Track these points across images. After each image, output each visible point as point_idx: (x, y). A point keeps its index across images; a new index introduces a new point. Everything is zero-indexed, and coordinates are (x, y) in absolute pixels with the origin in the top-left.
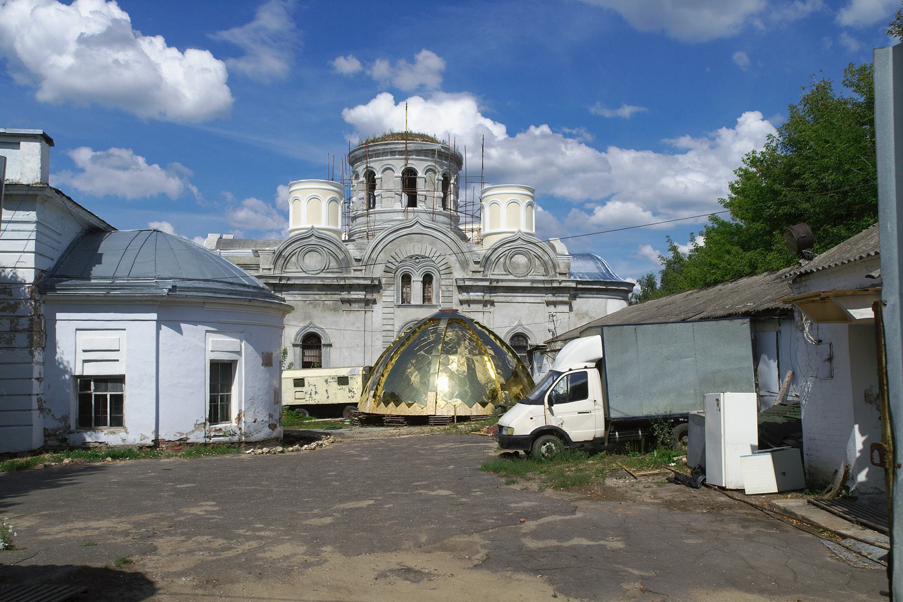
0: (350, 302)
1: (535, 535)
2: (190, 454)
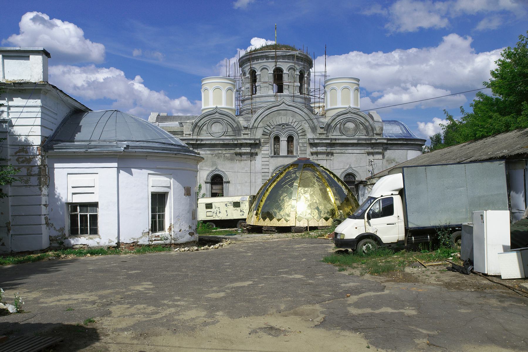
0: (241, 154)
1: (357, 305)
2: (139, 252)
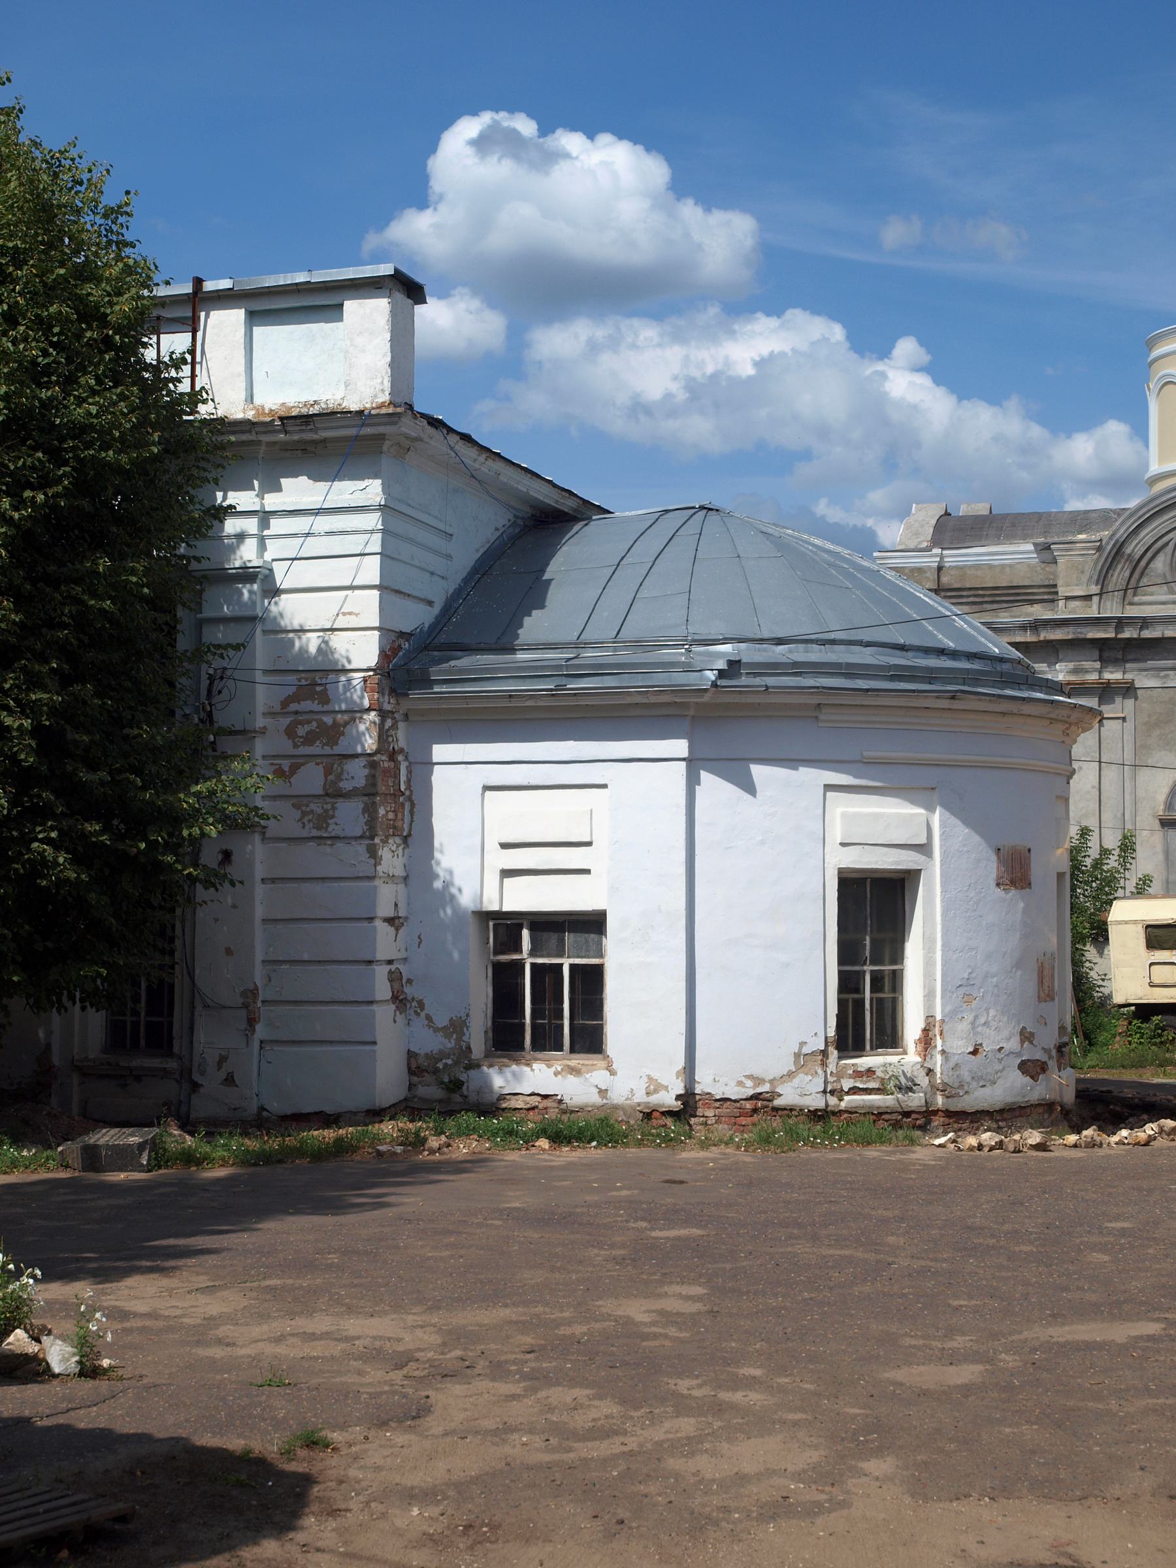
2: (766, 1140)
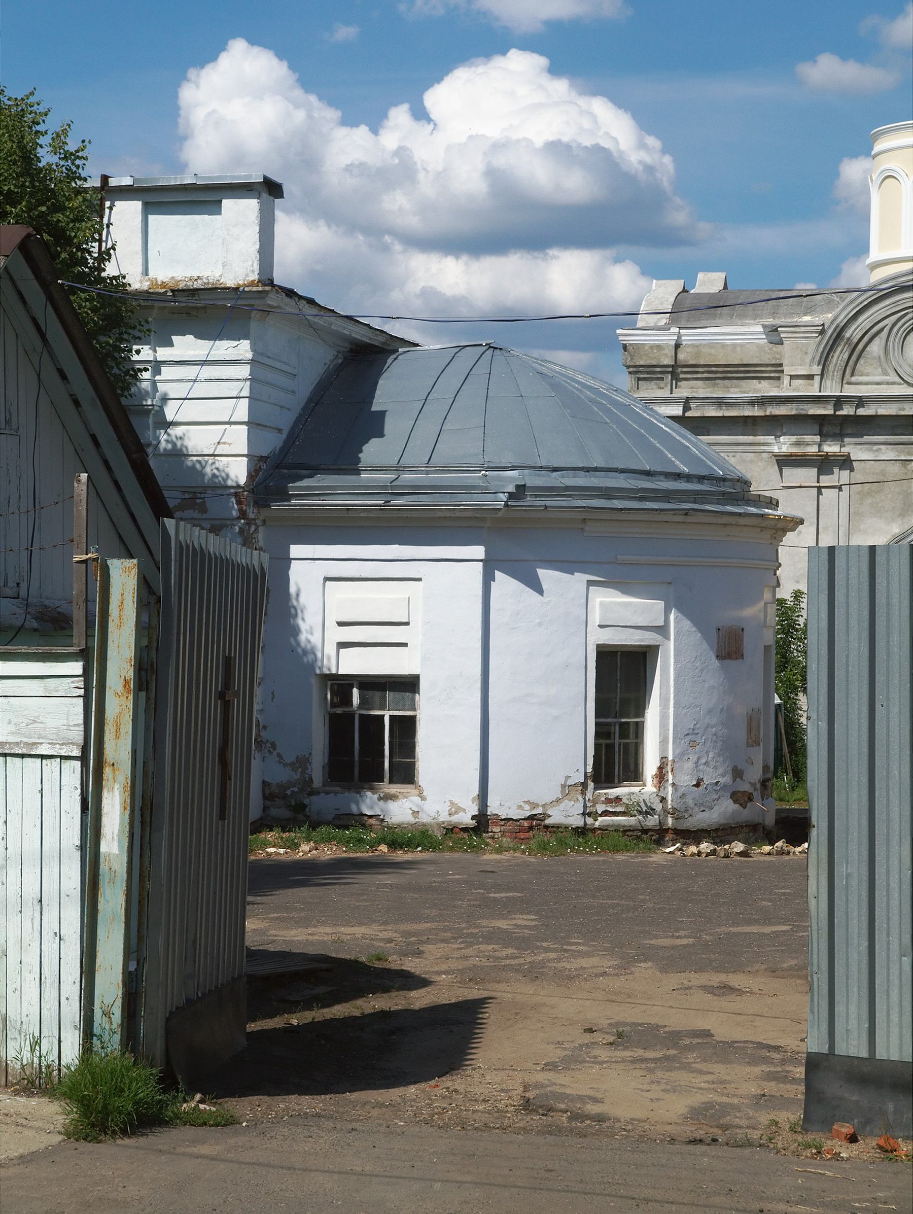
2: (544, 847)
